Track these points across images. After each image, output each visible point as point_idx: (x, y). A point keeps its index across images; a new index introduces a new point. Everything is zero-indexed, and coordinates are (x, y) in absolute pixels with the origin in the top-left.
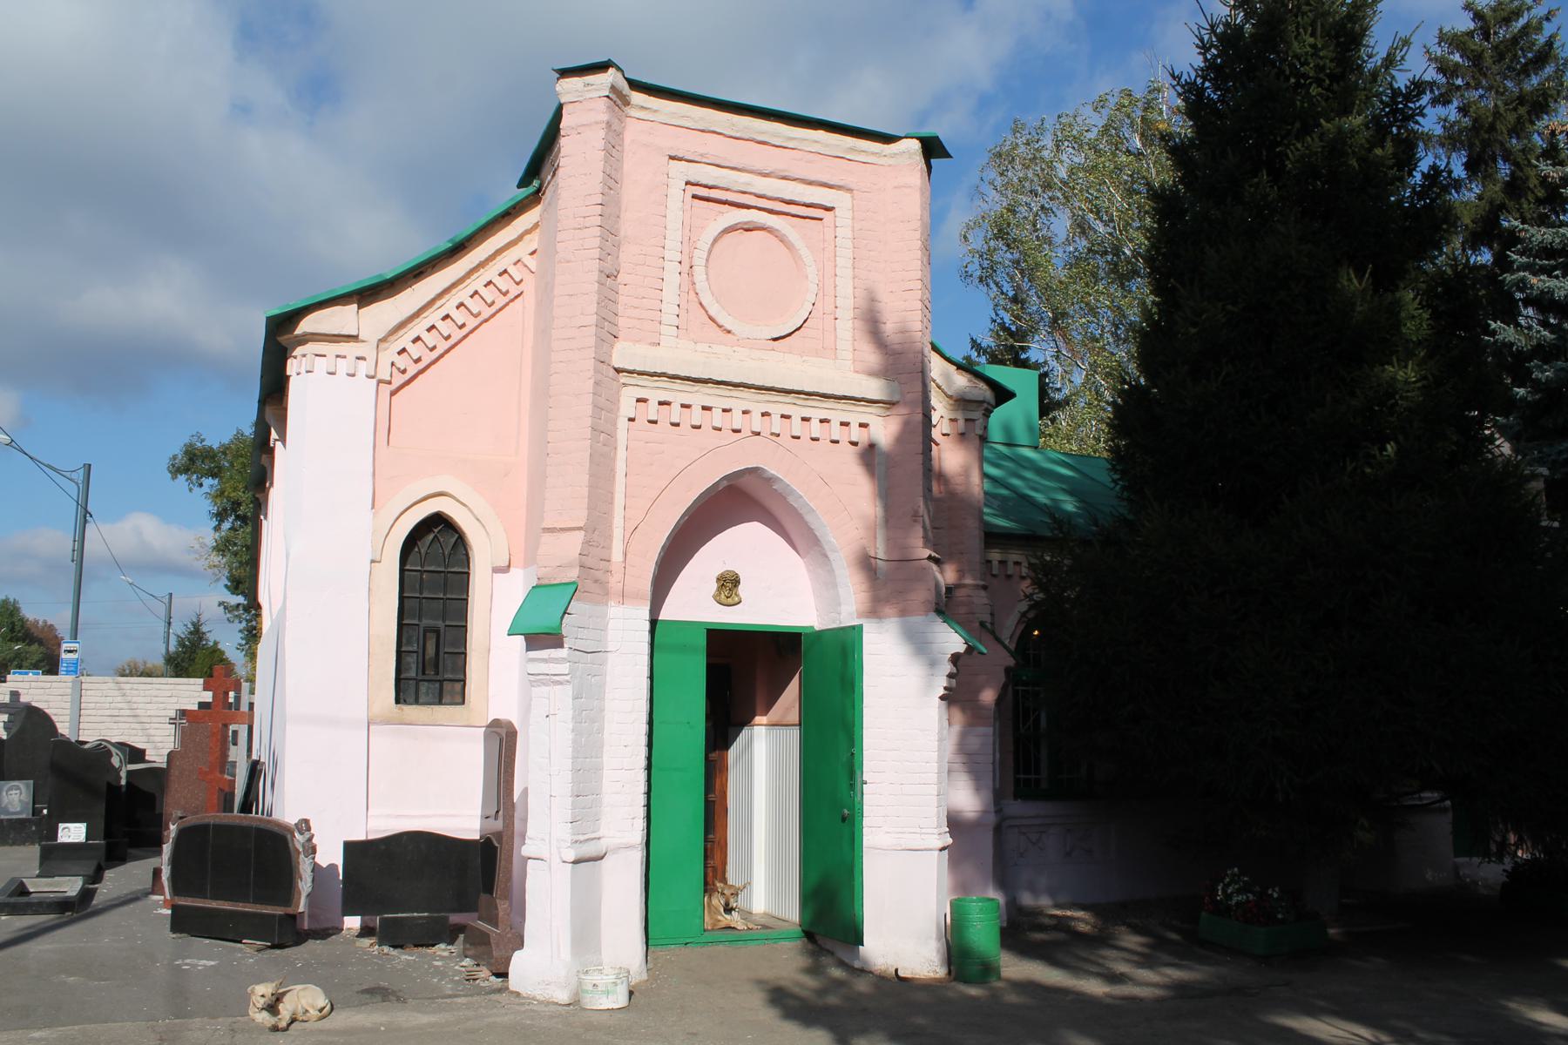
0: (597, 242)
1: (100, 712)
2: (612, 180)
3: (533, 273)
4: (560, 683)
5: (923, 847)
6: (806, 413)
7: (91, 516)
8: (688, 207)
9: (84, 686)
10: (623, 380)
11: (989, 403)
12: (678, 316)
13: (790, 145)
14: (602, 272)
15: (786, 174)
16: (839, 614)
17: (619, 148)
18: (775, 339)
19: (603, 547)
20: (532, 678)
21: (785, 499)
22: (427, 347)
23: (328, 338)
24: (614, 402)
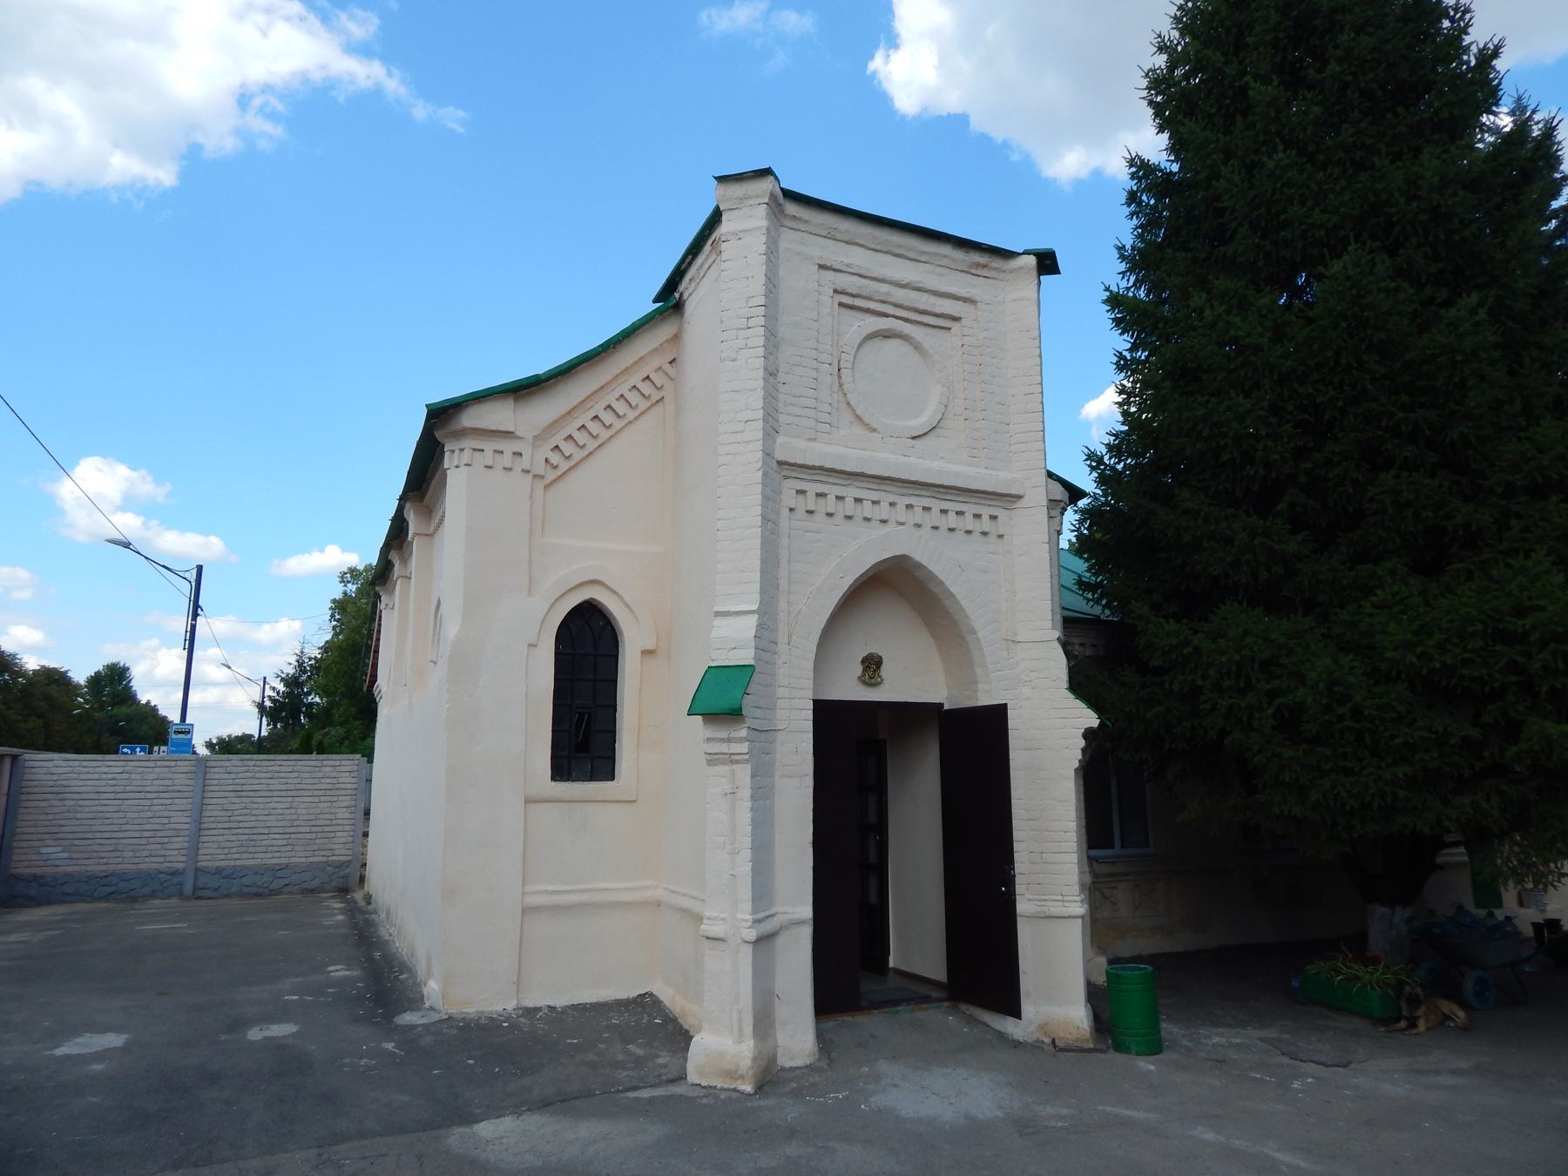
0: (761, 341)
1: (224, 788)
3: (672, 380)
4: (737, 762)
8: (836, 313)
10: (785, 473)
11: (1065, 503)
13: (923, 258)
15: (920, 285)
17: (776, 255)
18: (914, 438)
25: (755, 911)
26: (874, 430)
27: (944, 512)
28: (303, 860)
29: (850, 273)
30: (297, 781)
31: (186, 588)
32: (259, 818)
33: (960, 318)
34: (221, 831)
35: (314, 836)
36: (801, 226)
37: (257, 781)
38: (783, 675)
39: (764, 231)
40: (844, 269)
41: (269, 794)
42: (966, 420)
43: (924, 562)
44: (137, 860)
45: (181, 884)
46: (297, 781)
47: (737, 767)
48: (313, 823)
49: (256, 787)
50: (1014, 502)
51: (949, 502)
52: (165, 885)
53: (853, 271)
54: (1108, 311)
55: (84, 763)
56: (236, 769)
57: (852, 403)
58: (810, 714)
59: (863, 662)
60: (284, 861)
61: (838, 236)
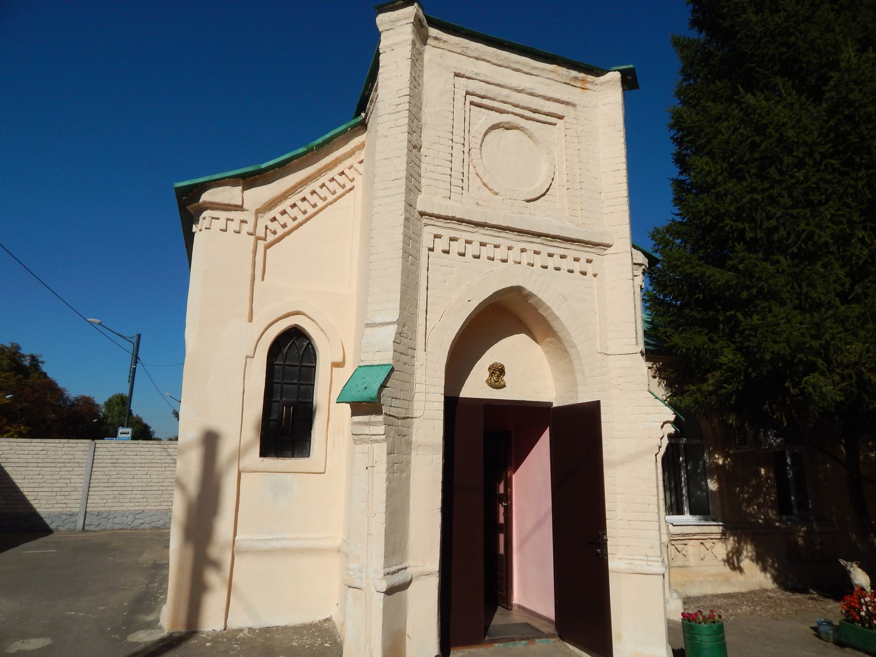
1: (105, 461)
2: (416, 82)
4: (377, 441)
5: (650, 572)
6: (551, 250)
7: (139, 360)
8: (467, 109)
9: (97, 446)
12: (337, 605)
13: (535, 72)
14: (410, 142)
15: (532, 91)
16: (576, 392)
18: (529, 201)
19: (411, 339)
20: (356, 437)
21: (536, 310)
22: (290, 217)
23: (221, 207)
24: (419, 235)
25: (387, 565)
26: (497, 194)
27: (551, 255)
28: (154, 508)
29: (478, 80)
30: (153, 457)
31: (130, 348)
32: (127, 480)
33: (564, 117)
34: (102, 489)
35: (161, 492)
36: (441, 45)
37: (127, 457)
38: (419, 375)
39: (410, 42)
40: (474, 76)
41: (134, 465)
42: (568, 189)
43: (535, 292)
44: (49, 506)
45: (75, 522)
46: (153, 457)
47: (375, 445)
48: (160, 484)
49: (126, 461)
50: (605, 250)
51: (555, 248)
52: (66, 522)
53: (481, 79)
54: (675, 165)
55: (19, 444)
56: (113, 450)
57: (479, 174)
58: (441, 406)
59: (489, 369)
60: (141, 508)
61: (469, 53)
